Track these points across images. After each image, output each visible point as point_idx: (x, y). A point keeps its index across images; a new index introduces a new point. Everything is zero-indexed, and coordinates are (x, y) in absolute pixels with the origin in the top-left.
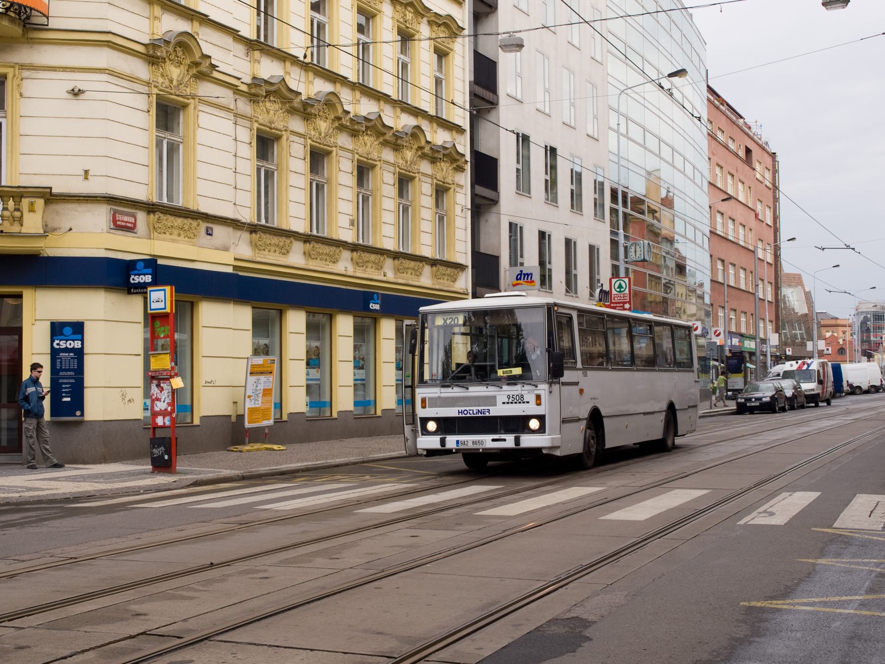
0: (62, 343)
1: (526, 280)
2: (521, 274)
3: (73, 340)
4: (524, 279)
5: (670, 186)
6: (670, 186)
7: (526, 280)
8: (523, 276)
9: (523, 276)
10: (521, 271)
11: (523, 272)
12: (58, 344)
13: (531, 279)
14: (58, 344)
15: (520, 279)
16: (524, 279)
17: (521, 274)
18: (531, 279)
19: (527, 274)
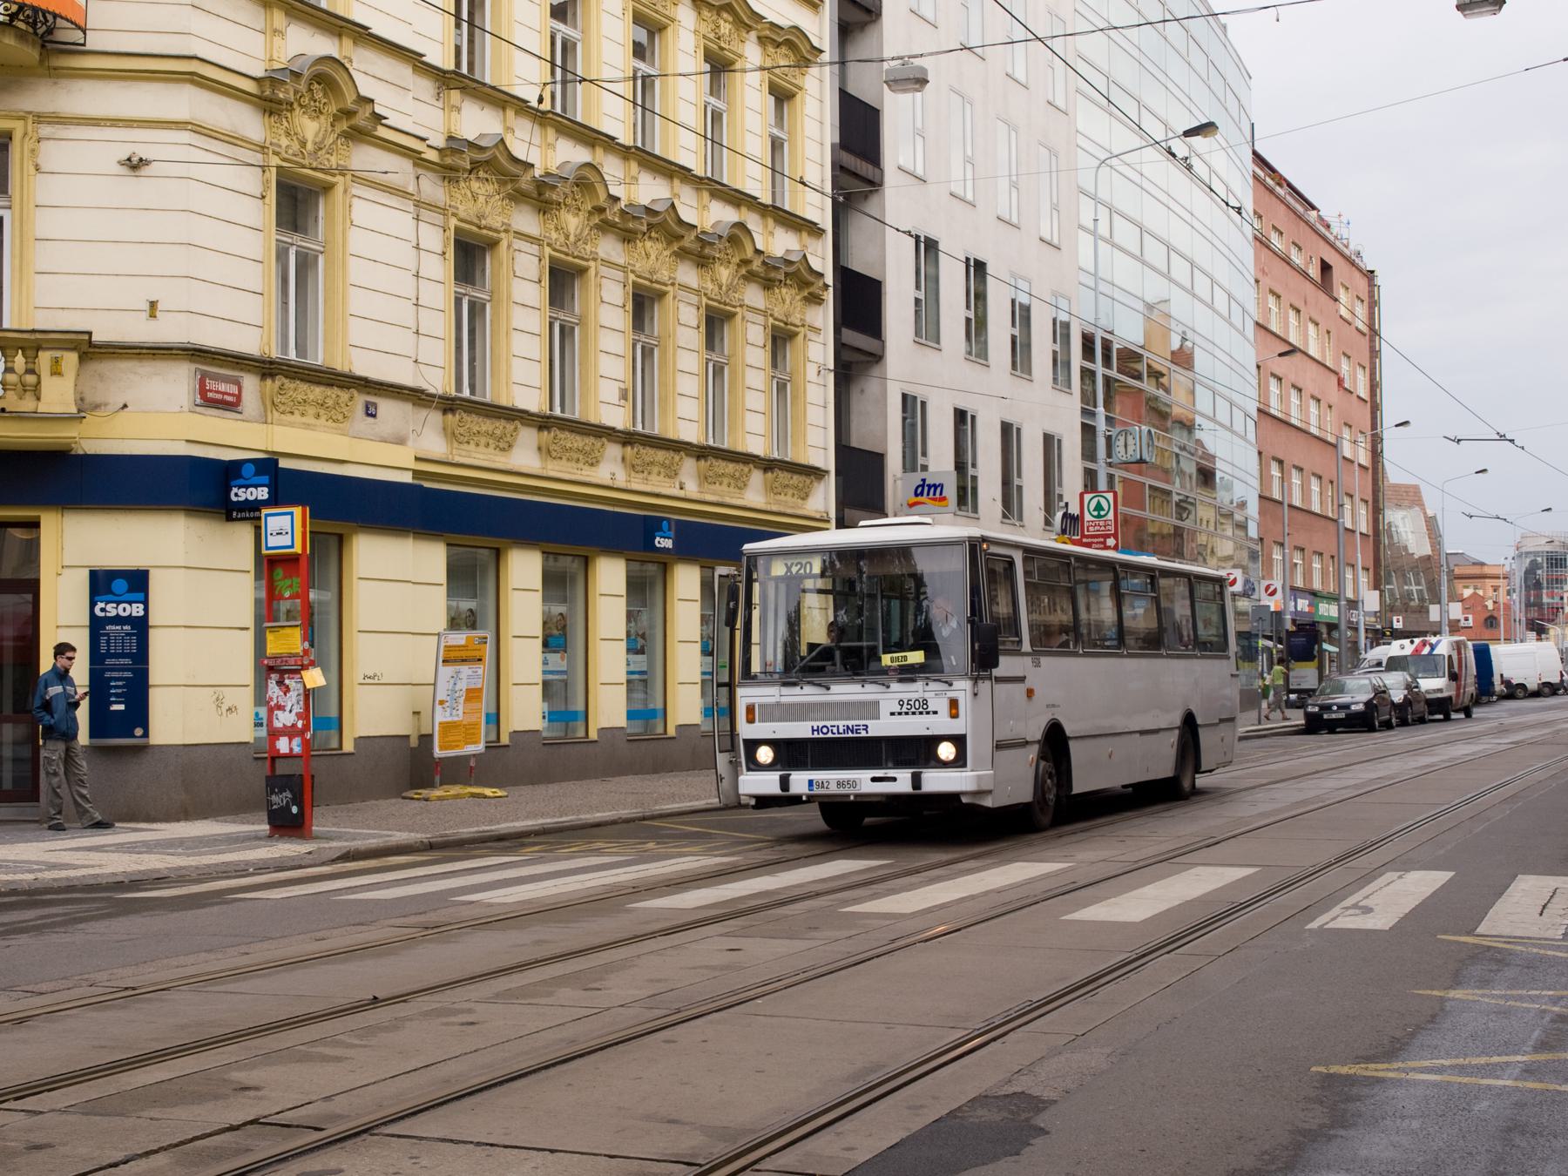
0: (109, 607)
1: (931, 495)
2: (923, 486)
3: (130, 603)
4: (928, 494)
5: (1187, 330)
6: (1187, 330)
7: (931, 495)
8: (926, 488)
9: (926, 488)
10: (924, 480)
11: (927, 483)
12: (103, 610)
13: (941, 493)
14: (103, 610)
15: (922, 494)
16: (928, 494)
17: (923, 486)
18: (941, 493)
19: (934, 485)
